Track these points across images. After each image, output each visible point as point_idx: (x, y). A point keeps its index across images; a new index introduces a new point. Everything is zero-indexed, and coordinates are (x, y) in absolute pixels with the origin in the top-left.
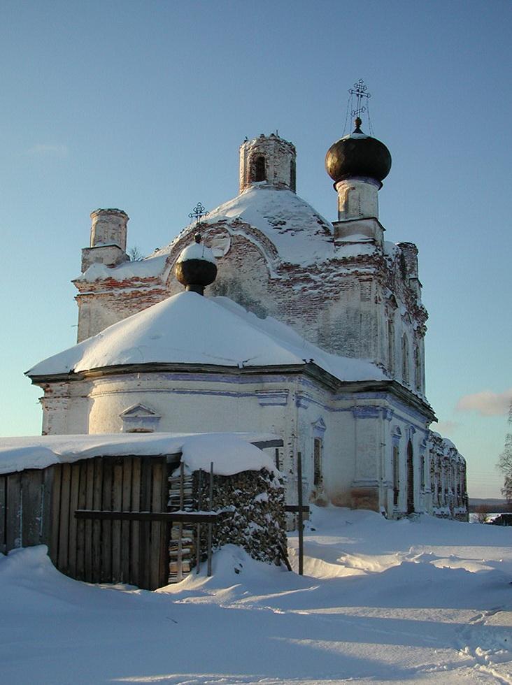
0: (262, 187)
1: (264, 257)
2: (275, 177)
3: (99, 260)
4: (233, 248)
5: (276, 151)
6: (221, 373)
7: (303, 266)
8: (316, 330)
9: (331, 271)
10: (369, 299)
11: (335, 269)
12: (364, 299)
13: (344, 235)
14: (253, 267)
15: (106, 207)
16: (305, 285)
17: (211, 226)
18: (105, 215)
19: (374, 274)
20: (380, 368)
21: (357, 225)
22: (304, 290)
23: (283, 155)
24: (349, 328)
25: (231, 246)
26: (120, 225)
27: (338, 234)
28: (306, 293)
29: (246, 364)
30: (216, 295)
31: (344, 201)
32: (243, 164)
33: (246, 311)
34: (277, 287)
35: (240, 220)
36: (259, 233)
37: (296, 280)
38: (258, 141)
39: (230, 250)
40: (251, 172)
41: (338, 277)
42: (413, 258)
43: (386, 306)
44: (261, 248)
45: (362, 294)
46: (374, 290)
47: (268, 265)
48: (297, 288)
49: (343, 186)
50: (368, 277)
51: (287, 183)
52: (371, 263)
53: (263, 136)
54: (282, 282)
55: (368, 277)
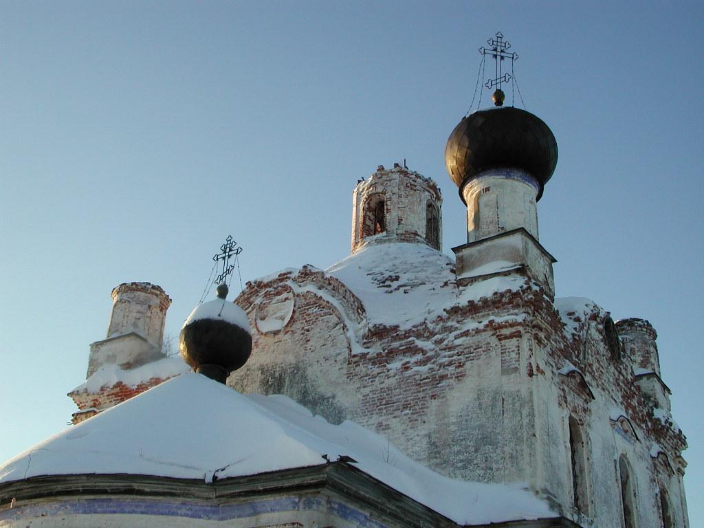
0: (379, 241)
1: (343, 322)
2: (399, 223)
3: (111, 359)
4: (297, 314)
5: (402, 187)
6: (172, 495)
7: (404, 327)
8: (425, 436)
9: (450, 329)
10: (516, 369)
11: (457, 325)
12: (508, 370)
13: (473, 266)
14: (326, 340)
15: (129, 282)
16: (408, 360)
17: (268, 285)
18: (127, 291)
19: (524, 324)
20: (542, 499)
21: (493, 246)
22: (406, 367)
23: (412, 192)
24: (481, 426)
25: (294, 312)
26: (150, 306)
27: (462, 267)
28: (409, 373)
29: (221, 475)
30: (267, 393)
31: (473, 214)
32: (354, 212)
33: (312, 415)
34: (362, 369)
35: (309, 268)
36: (336, 284)
37: (392, 354)
38: (375, 176)
39: (292, 318)
40: (364, 223)
41: (464, 338)
42: (646, 343)
43: (563, 390)
44: (340, 308)
45: (503, 362)
46: (525, 352)
47: (350, 334)
48: (396, 365)
49: (473, 189)
50: (514, 330)
51: (419, 233)
52: (518, 306)
53: (381, 168)
54: (370, 360)
55: (514, 330)
